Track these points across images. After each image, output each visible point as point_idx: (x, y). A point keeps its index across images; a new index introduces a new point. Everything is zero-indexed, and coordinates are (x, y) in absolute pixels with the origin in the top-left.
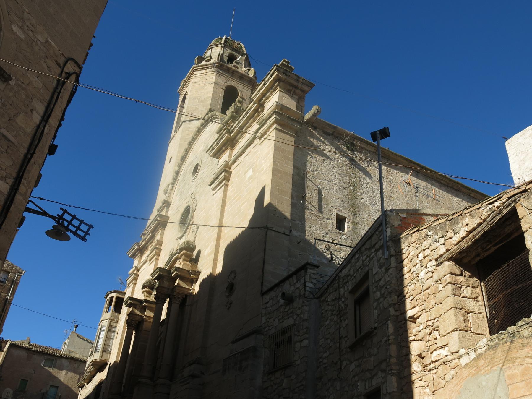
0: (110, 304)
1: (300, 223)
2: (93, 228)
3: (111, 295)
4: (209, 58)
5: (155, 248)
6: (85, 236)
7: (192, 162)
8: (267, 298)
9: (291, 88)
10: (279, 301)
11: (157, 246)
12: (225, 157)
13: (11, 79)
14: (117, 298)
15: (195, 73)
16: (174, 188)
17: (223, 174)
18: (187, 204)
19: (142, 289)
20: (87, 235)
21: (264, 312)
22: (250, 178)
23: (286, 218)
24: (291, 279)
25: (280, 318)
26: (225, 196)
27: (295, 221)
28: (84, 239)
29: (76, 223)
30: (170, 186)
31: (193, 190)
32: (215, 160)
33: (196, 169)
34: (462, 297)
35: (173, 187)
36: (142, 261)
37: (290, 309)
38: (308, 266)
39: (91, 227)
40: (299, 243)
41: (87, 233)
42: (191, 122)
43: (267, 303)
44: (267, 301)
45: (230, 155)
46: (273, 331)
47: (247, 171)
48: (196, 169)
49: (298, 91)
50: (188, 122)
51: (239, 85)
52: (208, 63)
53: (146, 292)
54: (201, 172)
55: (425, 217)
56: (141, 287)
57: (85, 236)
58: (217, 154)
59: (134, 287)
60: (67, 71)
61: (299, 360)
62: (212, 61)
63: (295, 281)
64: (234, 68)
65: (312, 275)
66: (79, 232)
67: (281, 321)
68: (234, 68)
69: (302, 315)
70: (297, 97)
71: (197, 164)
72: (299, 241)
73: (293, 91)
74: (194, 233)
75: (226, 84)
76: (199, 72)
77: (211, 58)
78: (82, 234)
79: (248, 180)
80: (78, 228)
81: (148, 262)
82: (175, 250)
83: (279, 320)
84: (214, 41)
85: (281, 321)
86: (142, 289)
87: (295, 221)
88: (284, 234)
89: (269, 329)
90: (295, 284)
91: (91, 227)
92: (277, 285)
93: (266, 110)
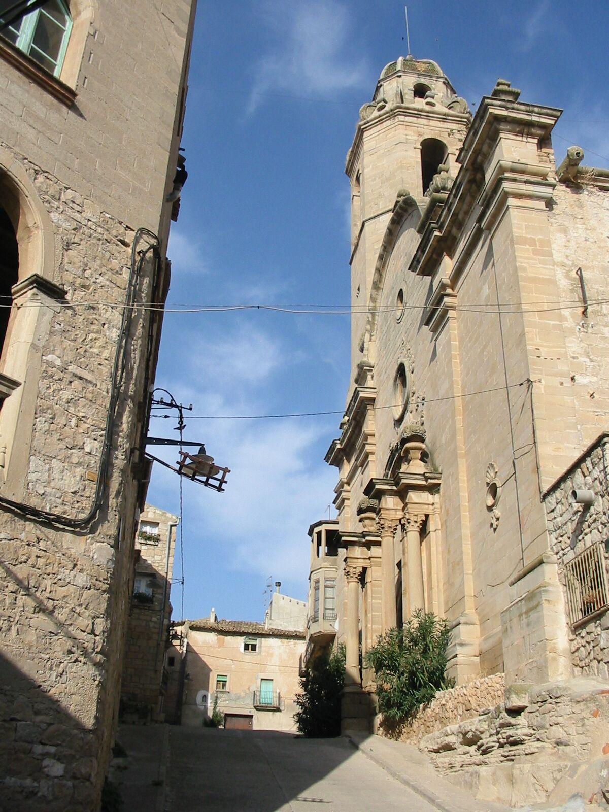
0: (319, 544)
2: (229, 471)
3: (316, 530)
4: (382, 103)
6: (221, 485)
8: (552, 500)
13: (66, 293)
14: (328, 531)
18: (399, 363)
19: (358, 515)
21: (550, 525)
23: (78, 726)
24: (583, 465)
27: (577, 358)
28: (219, 489)
34: (362, 679)
39: (226, 471)
41: (222, 481)
42: (377, 219)
44: (553, 507)
47: (481, 288)
50: (373, 221)
52: (383, 112)
57: (221, 485)
60: (139, 250)
62: (387, 109)
64: (427, 108)
66: (211, 481)
68: (427, 108)
70: (536, 141)
75: (421, 139)
76: (371, 131)
77: (386, 102)
78: (217, 483)
86: (358, 515)
87: (577, 358)
92: (563, 479)
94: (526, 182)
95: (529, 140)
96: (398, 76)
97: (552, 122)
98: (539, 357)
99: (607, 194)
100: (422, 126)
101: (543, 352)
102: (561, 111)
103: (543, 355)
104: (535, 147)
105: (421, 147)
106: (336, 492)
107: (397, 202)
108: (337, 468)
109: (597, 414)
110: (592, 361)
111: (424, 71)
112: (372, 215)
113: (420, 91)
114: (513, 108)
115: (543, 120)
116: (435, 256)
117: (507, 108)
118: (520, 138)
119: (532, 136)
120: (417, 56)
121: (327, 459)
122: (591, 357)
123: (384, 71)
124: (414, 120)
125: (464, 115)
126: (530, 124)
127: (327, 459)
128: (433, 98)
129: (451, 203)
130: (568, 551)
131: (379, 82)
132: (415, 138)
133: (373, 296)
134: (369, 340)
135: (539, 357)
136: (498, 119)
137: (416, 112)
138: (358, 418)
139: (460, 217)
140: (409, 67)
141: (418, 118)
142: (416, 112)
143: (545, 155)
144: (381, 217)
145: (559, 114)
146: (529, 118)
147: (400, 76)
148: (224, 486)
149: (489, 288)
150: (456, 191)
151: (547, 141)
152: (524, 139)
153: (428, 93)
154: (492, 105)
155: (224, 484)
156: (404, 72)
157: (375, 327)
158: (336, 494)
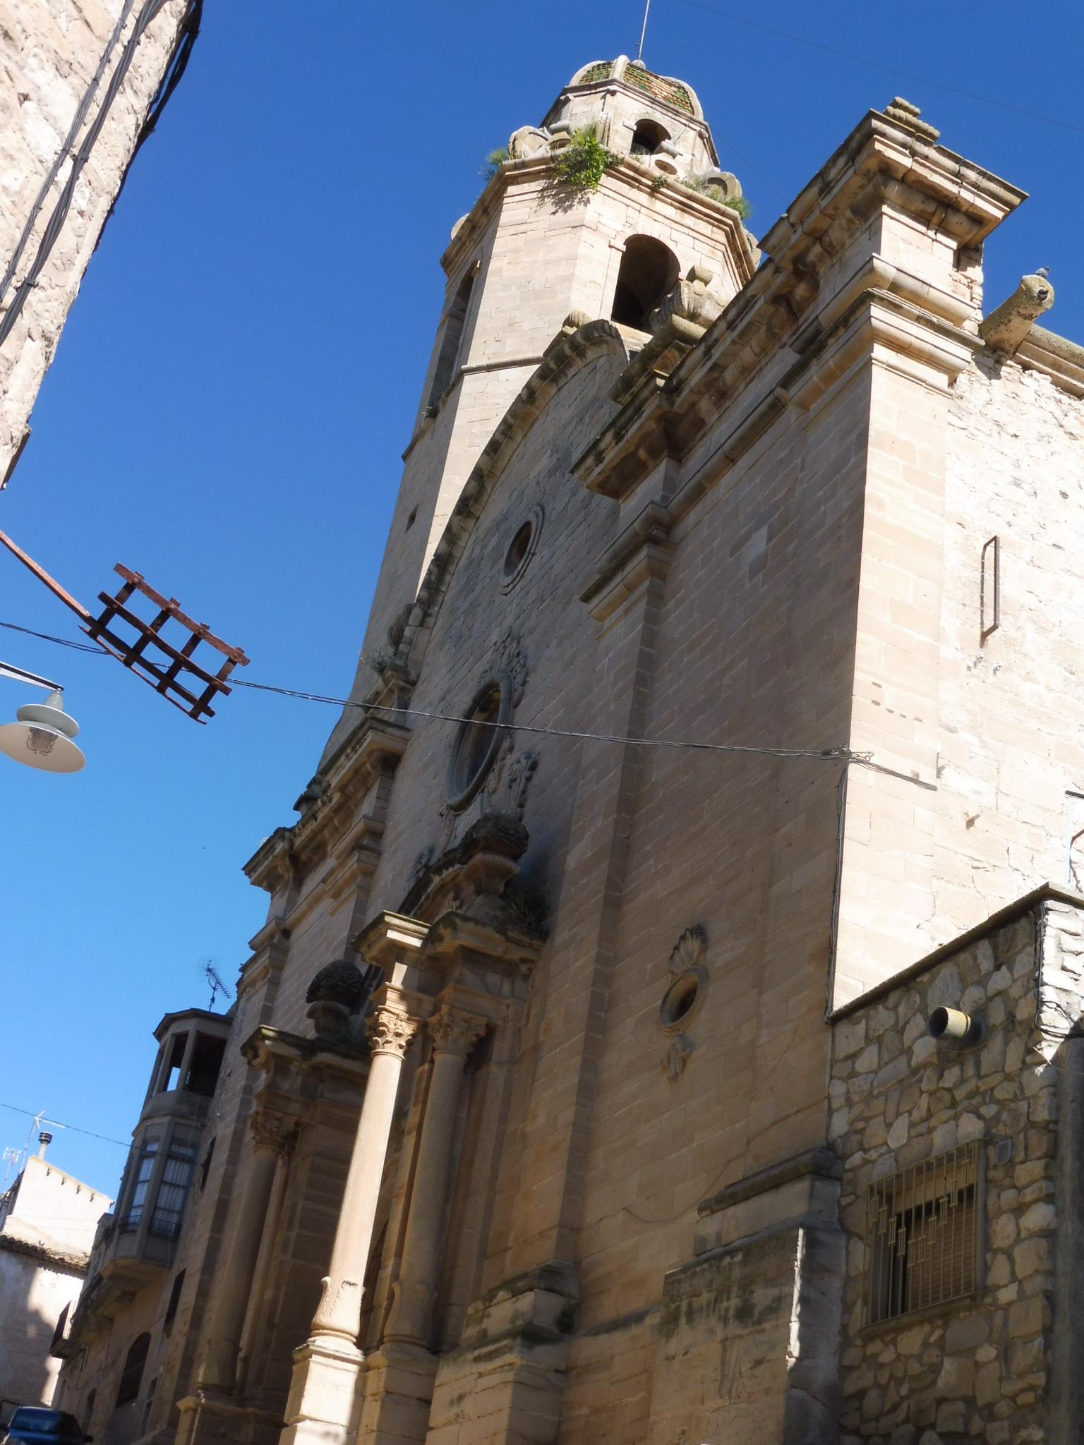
1: (976, 741)
2: (245, 662)
3: (176, 1028)
5: (357, 846)
7: (505, 518)
9: (931, 207)
10: (909, 1052)
11: (365, 842)
12: (649, 488)
15: (511, 190)
16: (430, 621)
17: (644, 552)
18: (487, 678)
20: (219, 694)
22: (759, 565)
25: (916, 1115)
26: (650, 637)
29: (174, 634)
30: (417, 612)
31: (509, 621)
32: (604, 502)
33: (522, 543)
35: (426, 614)
36: (301, 899)
37: (962, 1081)
38: (1050, 903)
39: (236, 658)
40: (970, 823)
43: (853, 1057)
45: (670, 485)
46: (883, 1169)
47: (747, 537)
48: (522, 543)
49: (956, 221)
51: (676, 236)
53: (327, 1011)
54: (540, 555)
55: (156, 1223)
56: (304, 991)
58: (619, 482)
59: (270, 997)
61: (1014, 1288)
63: (986, 964)
64: (658, 173)
65: (1065, 937)
67: (922, 1128)
68: (658, 173)
69: (1023, 1106)
70: (954, 245)
71: (528, 524)
72: (972, 815)
73: (935, 220)
74: (518, 787)
79: (753, 572)
80: (181, 662)
81: (327, 903)
82: (438, 854)
83: (912, 1125)
84: (589, 66)
85: (922, 1128)
88: (915, 780)
89: (866, 1162)
90: (988, 975)
91: (236, 658)
93: (826, 294)
94: (918, 319)
95: (940, 237)
96: (608, 91)
97: (1000, 214)
98: (878, 704)
99: (1077, 404)
100: (638, 207)
101: (889, 695)
102: (1023, 197)
103: (886, 703)
104: (949, 257)
105: (624, 248)
106: (252, 947)
107: (562, 334)
108: (268, 894)
109: (976, 864)
110: (984, 745)
111: (665, 98)
112: (484, 363)
113: (648, 137)
114: (926, 158)
115: (979, 203)
116: (642, 454)
117: (914, 154)
118: (922, 228)
119: (943, 229)
120: (657, 67)
121: (249, 869)
122: (984, 738)
123: (582, 72)
124: (624, 188)
125: (730, 210)
126: (948, 204)
127: (249, 869)
128: (674, 156)
129: (717, 341)
130: (881, 1155)
131: (565, 91)
132: (620, 228)
133: (454, 529)
134: (418, 622)
135: (878, 704)
136: (887, 170)
137: (631, 173)
138: (351, 788)
139: (729, 375)
140: (637, 82)
141: (631, 185)
142: (631, 173)
143: (965, 281)
144: (503, 373)
145: (1016, 200)
146: (954, 189)
147: (613, 93)
148: (217, 701)
149: (770, 539)
150: (739, 314)
151: (972, 254)
152: (931, 233)
153: (666, 144)
154: (883, 135)
155: (219, 694)
156: (625, 87)
157: (440, 599)
158: (253, 953)
